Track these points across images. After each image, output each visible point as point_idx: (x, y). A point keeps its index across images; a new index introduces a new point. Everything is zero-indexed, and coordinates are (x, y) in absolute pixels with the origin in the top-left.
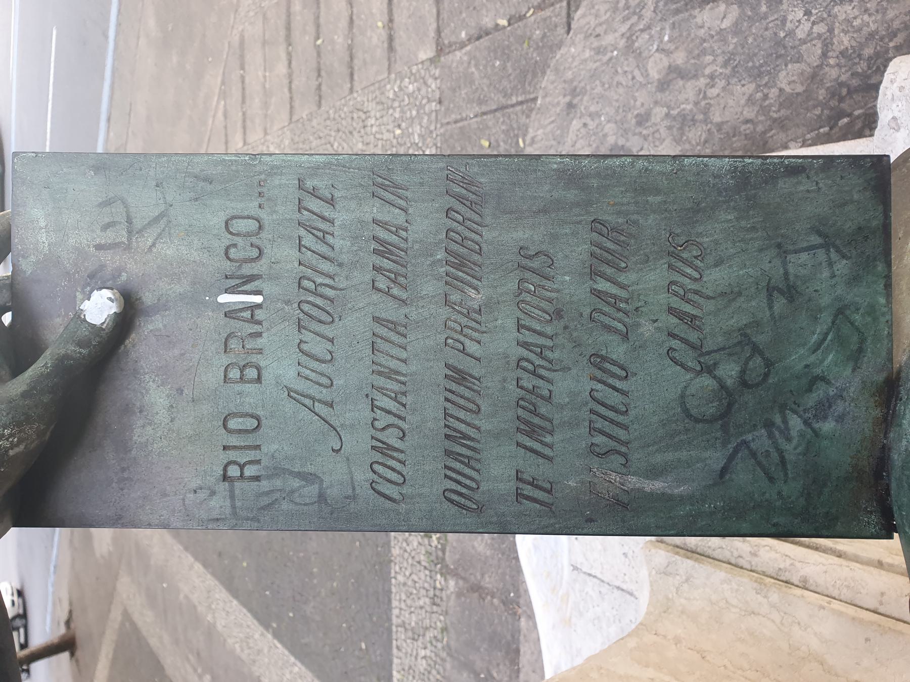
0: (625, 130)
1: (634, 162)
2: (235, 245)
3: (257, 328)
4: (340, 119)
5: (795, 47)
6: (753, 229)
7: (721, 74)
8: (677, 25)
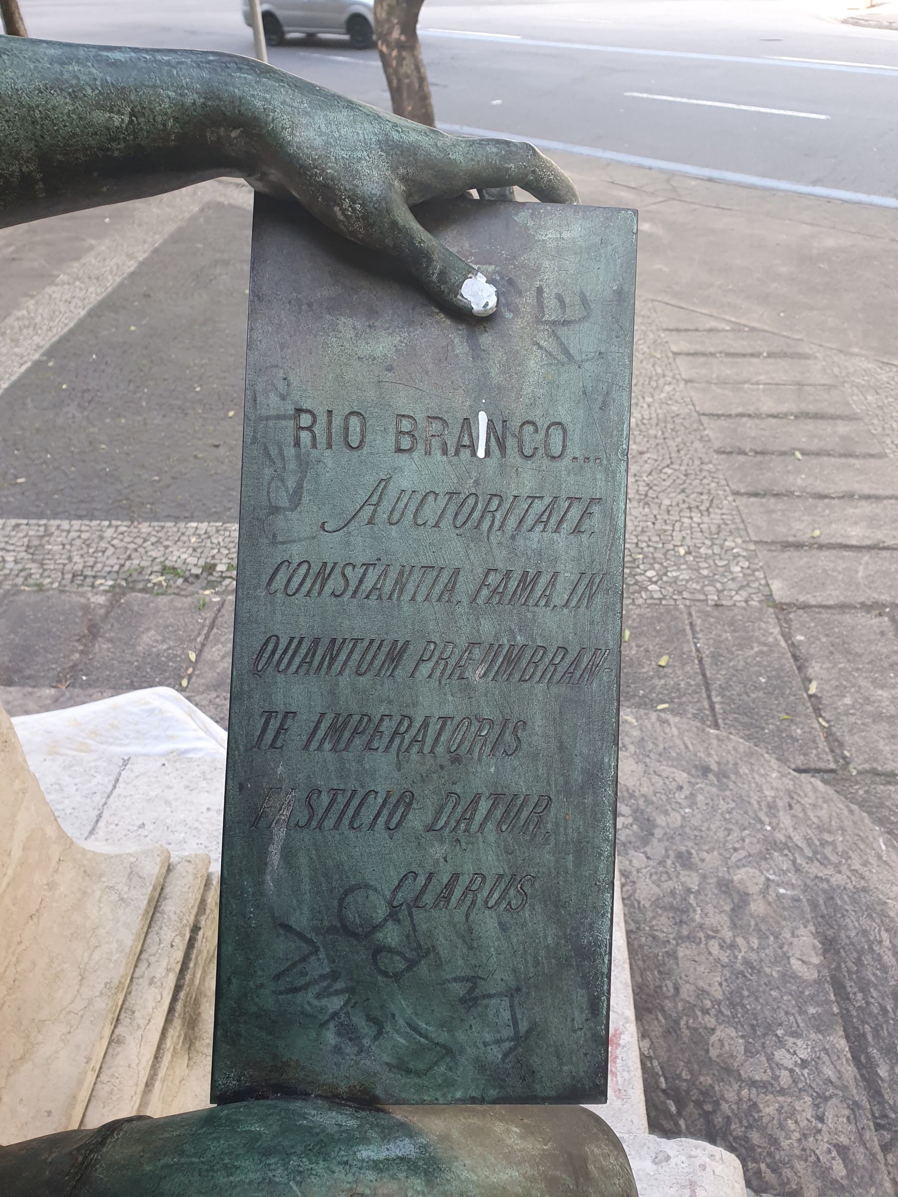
0: (672, 838)
1: (609, 841)
2: (536, 431)
3: (452, 450)
4: (701, 477)
5: (764, 1047)
6: (537, 963)
7: (736, 957)
8: (797, 904)
